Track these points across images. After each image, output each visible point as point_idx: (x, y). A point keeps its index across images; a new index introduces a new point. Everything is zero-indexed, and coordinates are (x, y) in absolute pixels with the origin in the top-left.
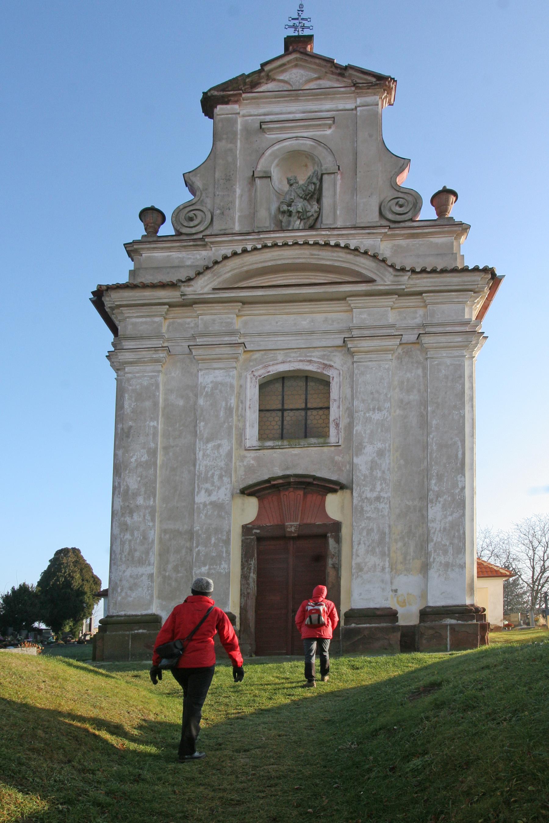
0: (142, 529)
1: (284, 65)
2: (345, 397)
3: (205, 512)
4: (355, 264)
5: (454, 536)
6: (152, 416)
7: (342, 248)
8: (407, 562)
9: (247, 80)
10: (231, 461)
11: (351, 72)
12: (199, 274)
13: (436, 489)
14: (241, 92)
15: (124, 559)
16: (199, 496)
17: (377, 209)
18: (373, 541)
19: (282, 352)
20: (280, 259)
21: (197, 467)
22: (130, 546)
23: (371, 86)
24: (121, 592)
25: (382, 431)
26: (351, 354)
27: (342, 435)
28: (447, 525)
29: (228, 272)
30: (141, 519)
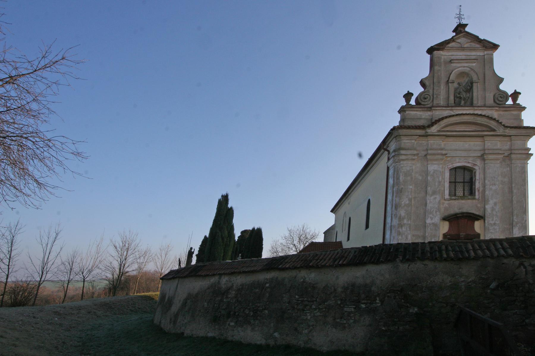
26: (484, 160)
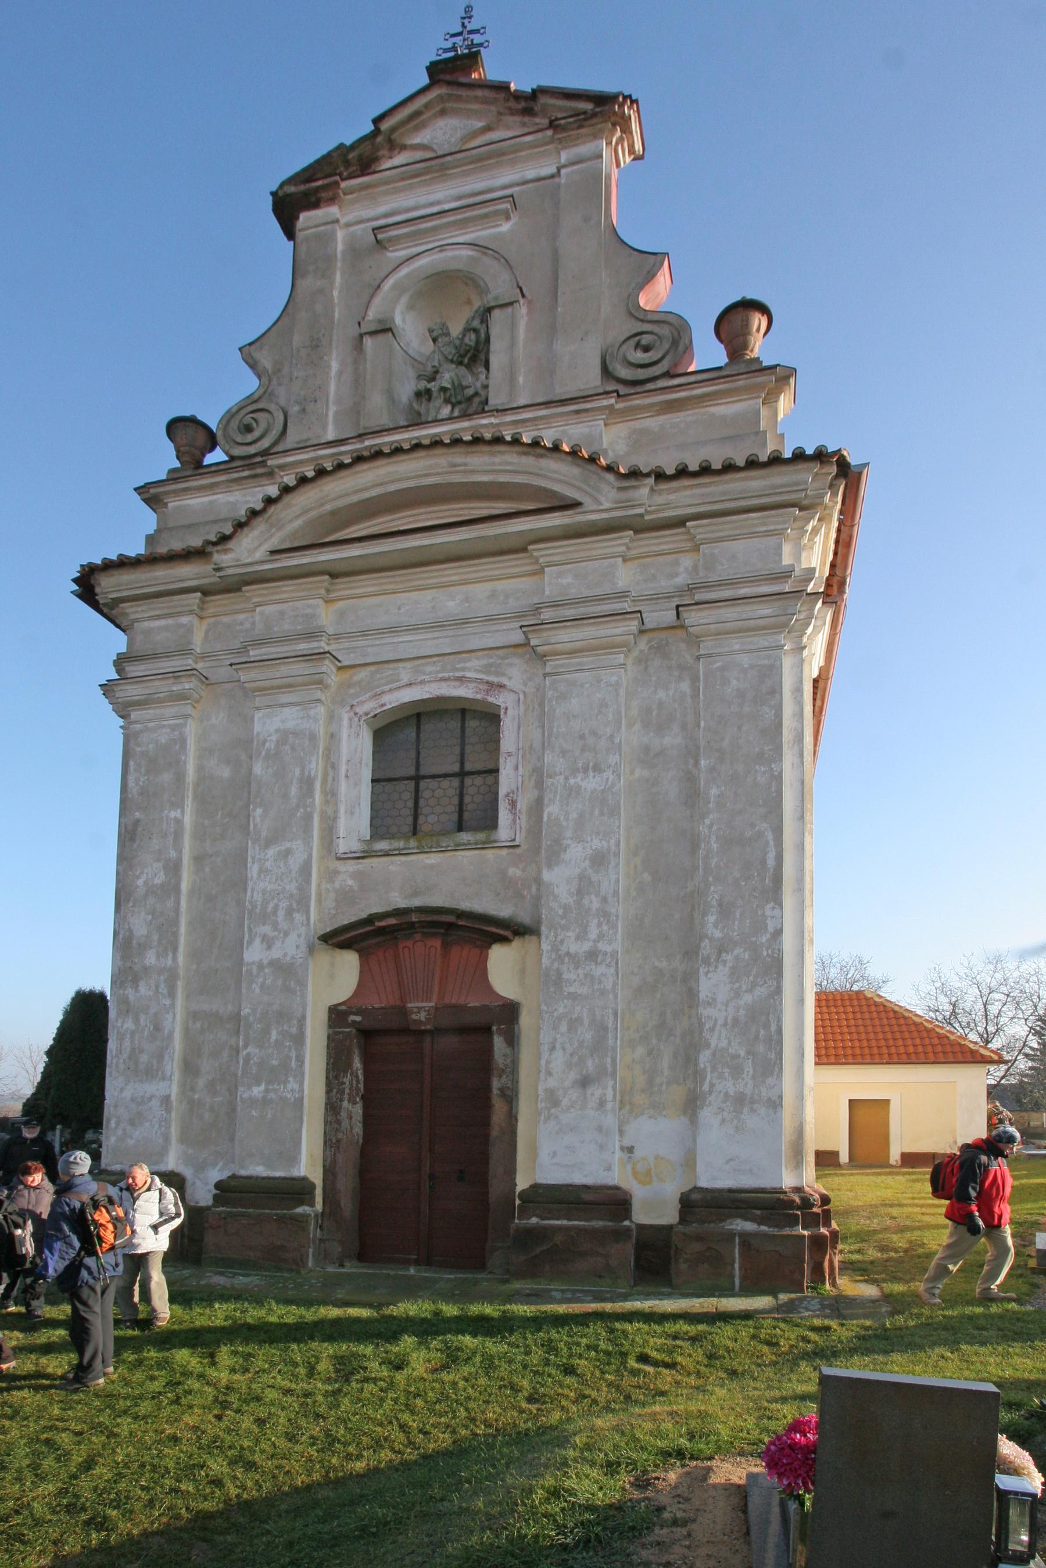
0: (152, 1011)
1: (417, 114)
2: (531, 746)
3: (261, 980)
4: (538, 475)
5: (757, 1038)
6: (173, 799)
7: (509, 443)
8: (656, 1089)
9: (351, 156)
10: (308, 881)
11: (544, 100)
12: (240, 526)
13: (718, 934)
14: (338, 178)
15: (122, 1066)
16: (250, 949)
17: (598, 362)
18: (581, 1044)
19: (408, 665)
20: (392, 482)
21: (249, 894)
22: (132, 1042)
23: (585, 120)
24: (116, 1128)
25: (602, 814)
27: (523, 821)
28: (742, 1012)
29: (298, 517)
30: (151, 993)
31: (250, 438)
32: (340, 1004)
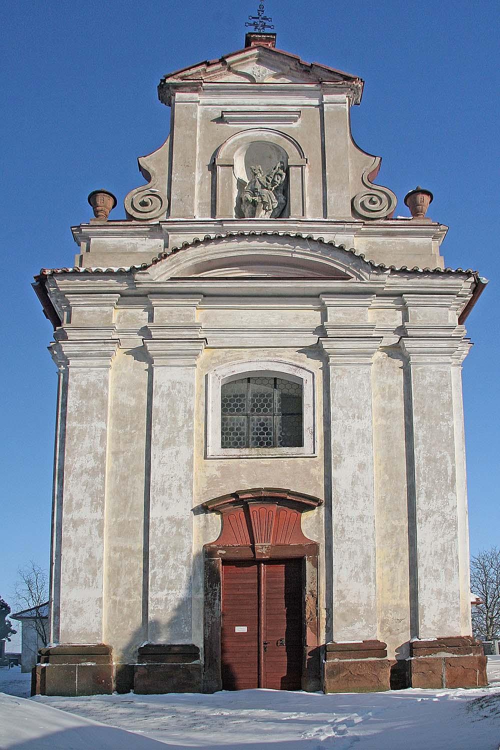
0: (88, 545)
12: (155, 262)
18: (356, 566)
31: (140, 208)
32: (212, 544)
